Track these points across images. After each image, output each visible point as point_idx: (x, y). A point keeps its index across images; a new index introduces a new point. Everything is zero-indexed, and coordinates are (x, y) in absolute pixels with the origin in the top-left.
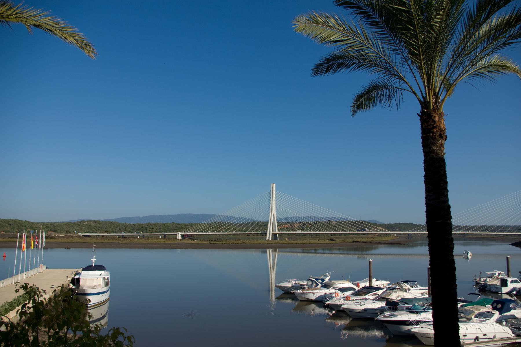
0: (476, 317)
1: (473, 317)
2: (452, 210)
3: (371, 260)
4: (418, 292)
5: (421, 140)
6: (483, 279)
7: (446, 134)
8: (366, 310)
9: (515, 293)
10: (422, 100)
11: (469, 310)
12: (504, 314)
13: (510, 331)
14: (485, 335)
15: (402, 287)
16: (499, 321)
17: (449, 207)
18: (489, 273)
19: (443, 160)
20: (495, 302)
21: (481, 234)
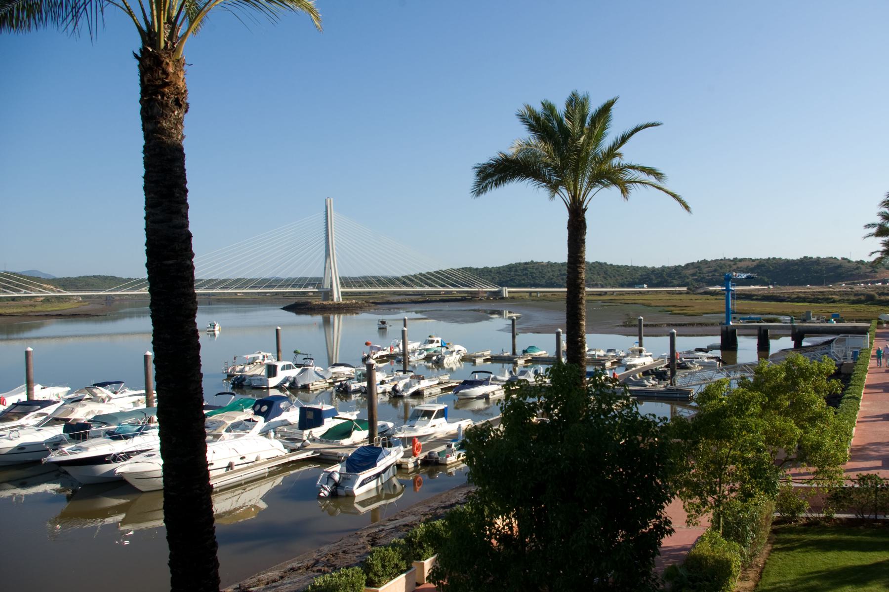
0: (228, 430)
1: (223, 432)
2: (194, 241)
3: (30, 349)
4: (126, 401)
5: (140, 106)
6: (238, 368)
7: (187, 101)
8: (21, 448)
9: (287, 385)
10: (144, 28)
11: (217, 421)
12: (272, 420)
13: (281, 446)
14: (242, 458)
15: (95, 395)
16: (265, 433)
17: (190, 236)
18: (249, 356)
19: (181, 150)
20: (258, 402)
21: (236, 294)
